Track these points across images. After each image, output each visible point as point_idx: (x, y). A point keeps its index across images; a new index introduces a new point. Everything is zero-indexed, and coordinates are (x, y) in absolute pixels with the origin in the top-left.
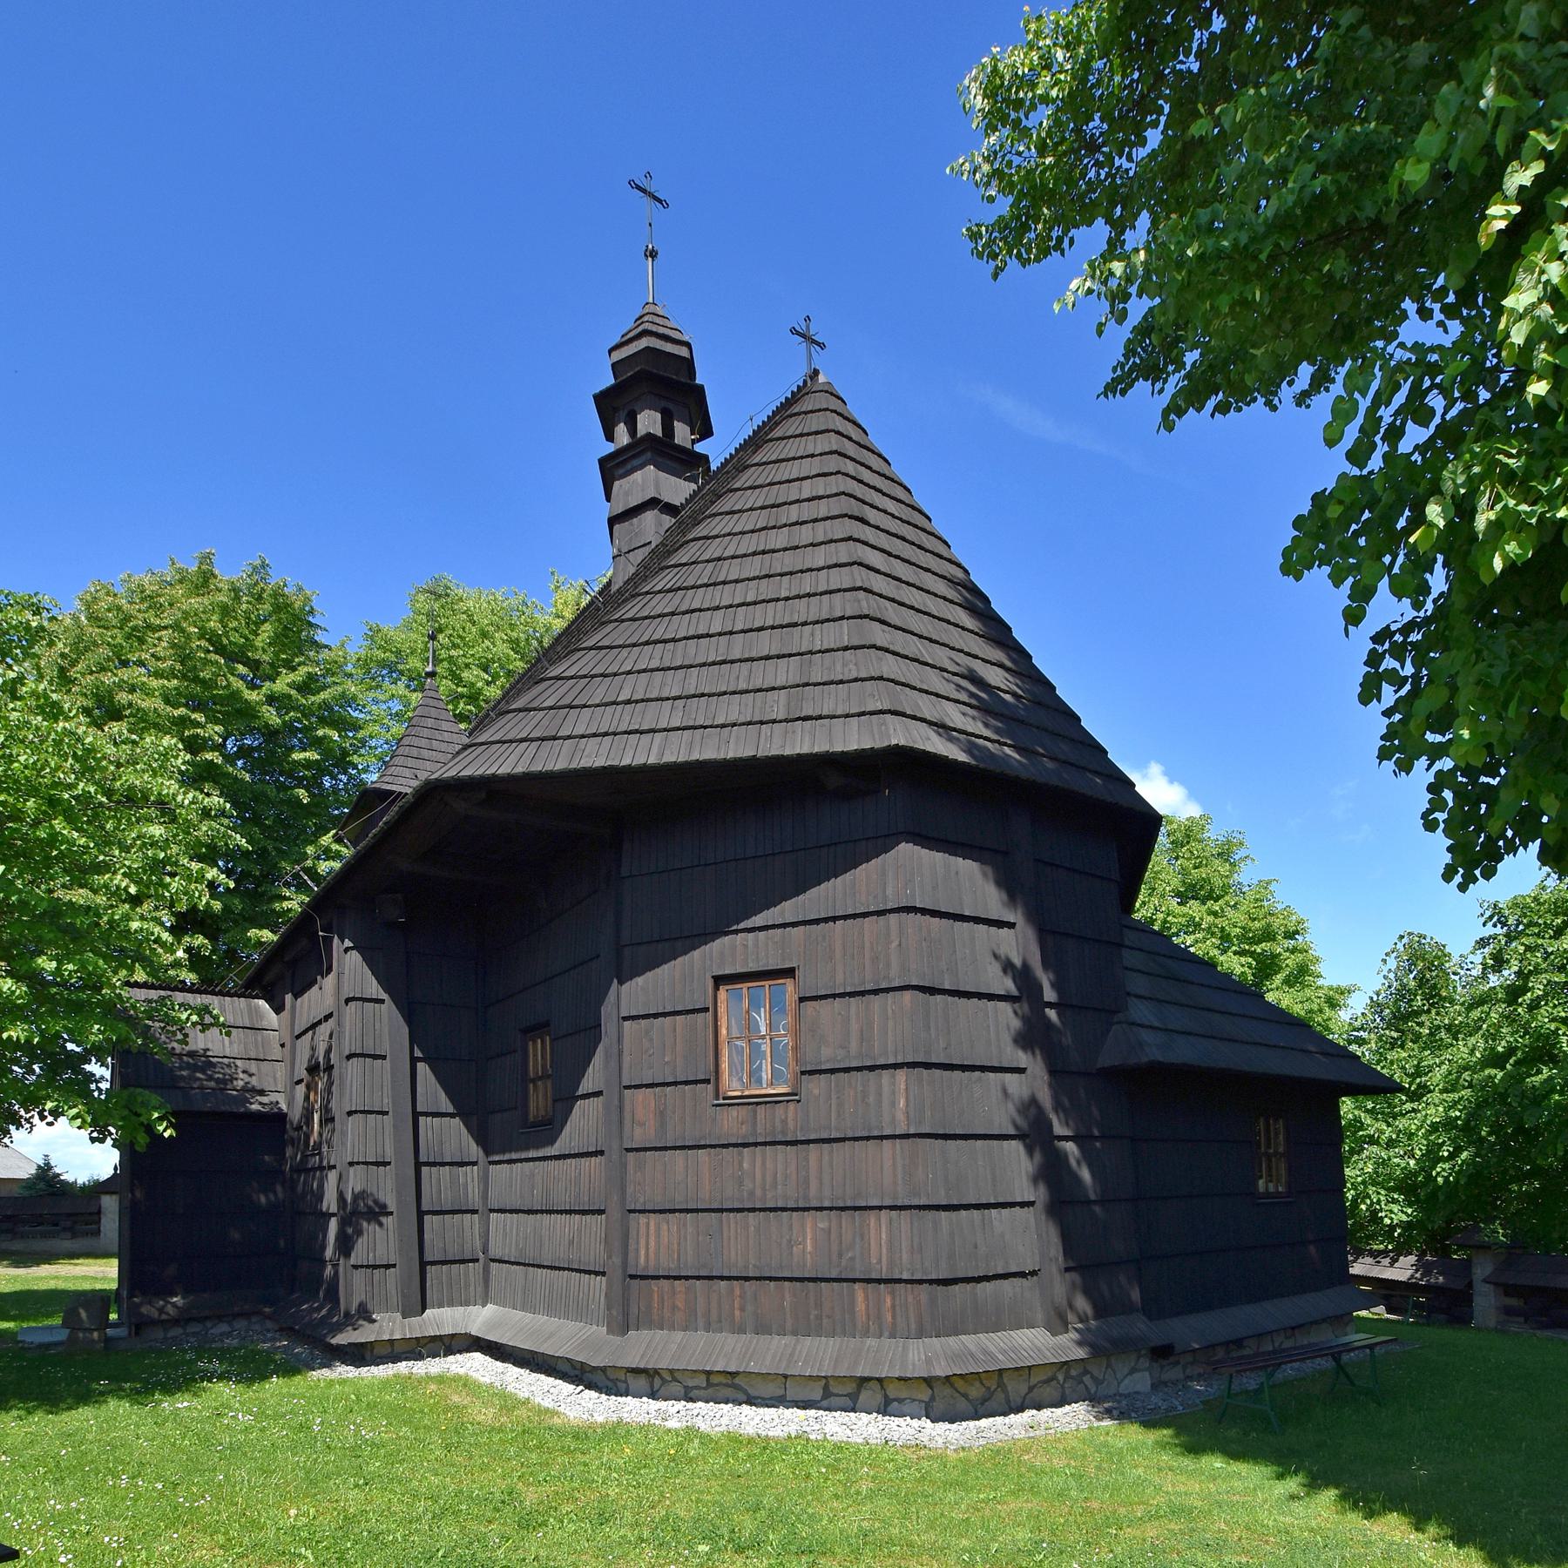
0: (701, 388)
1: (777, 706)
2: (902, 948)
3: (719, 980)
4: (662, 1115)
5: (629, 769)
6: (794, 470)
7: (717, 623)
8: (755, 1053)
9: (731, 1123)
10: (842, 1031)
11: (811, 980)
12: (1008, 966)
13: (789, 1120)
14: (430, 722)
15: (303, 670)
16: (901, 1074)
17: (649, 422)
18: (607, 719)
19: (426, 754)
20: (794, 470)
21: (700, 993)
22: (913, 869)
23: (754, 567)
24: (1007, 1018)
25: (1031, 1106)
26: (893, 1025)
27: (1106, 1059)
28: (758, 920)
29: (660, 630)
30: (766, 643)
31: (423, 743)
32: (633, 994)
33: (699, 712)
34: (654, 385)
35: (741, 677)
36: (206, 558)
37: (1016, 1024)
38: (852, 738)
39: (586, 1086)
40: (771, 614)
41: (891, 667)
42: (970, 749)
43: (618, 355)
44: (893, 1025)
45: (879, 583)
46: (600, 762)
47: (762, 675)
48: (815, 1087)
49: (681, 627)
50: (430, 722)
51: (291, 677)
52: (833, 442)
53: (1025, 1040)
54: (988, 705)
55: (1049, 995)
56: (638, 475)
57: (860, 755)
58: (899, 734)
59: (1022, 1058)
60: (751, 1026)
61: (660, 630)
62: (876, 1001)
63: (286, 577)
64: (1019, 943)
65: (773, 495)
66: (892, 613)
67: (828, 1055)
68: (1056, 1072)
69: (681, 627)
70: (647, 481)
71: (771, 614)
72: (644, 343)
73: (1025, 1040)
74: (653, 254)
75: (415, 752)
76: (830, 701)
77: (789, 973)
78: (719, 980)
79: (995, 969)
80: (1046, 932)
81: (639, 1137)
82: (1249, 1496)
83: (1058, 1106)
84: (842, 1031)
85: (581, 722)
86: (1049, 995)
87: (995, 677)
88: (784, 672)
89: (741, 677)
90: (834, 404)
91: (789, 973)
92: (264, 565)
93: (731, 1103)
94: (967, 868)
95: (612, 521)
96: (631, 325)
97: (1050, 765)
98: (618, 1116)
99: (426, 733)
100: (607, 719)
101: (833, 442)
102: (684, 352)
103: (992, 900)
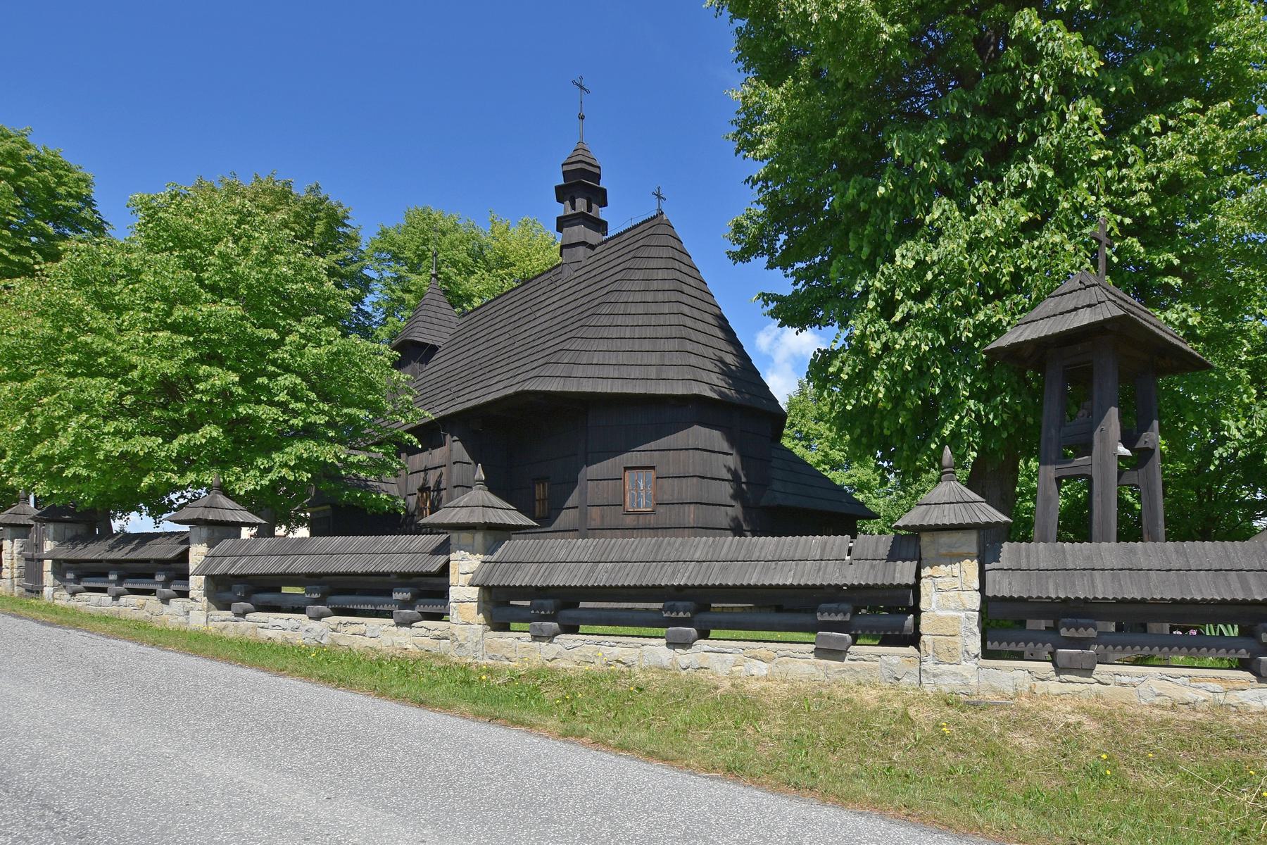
0: (605, 191)
1: (652, 373)
2: (694, 462)
3: (626, 469)
4: (602, 517)
5: (792, 587)
6: (653, 263)
7: (627, 333)
8: (639, 496)
9: (630, 521)
10: (671, 490)
11: (661, 471)
12: (729, 470)
13: (652, 520)
14: (435, 303)
15: (343, 254)
16: (692, 507)
17: (581, 205)
18: (591, 371)
19: (435, 321)
20: (653, 263)
21: (619, 472)
22: (699, 435)
23: (641, 309)
24: (728, 489)
25: (735, 519)
26: (689, 489)
27: (764, 502)
28: (641, 448)
29: (605, 333)
30: (647, 345)
31: (432, 314)
32: (593, 470)
33: (624, 372)
34: (581, 186)
35: (638, 358)
36: (288, 184)
37: (731, 491)
38: (680, 389)
39: (569, 503)
40: (648, 332)
41: (693, 360)
42: (720, 393)
43: (566, 168)
44: (689, 489)
45: (689, 322)
46: (589, 390)
47: (647, 359)
48: (662, 509)
49: (614, 332)
50: (435, 303)
51: (335, 257)
52: (670, 253)
53: (734, 497)
54: (726, 372)
55: (744, 479)
56: (575, 228)
57: (683, 395)
58: (696, 389)
59: (733, 503)
60: (638, 486)
61: (605, 333)
62: (684, 480)
63: (334, 196)
64: (733, 461)
65: (648, 274)
66: (693, 335)
67: (666, 498)
68: (745, 507)
69: (614, 332)
70: (579, 232)
71: (648, 332)
72: (579, 166)
73: (734, 497)
74: (582, 118)
75: (429, 320)
76: (672, 372)
77: (653, 468)
78: (626, 469)
79: (724, 471)
80: (744, 457)
81: (593, 524)
82: (900, 832)
83: (745, 520)
84: (671, 490)
85: (578, 371)
86: (744, 479)
87: (730, 359)
88: (654, 359)
89: (638, 358)
90: (668, 231)
91: (653, 468)
92: (317, 187)
93: (629, 513)
94: (717, 434)
95: (562, 247)
96: (570, 153)
97: (747, 396)
98: (584, 517)
99: (433, 309)
100: (591, 371)
101: (670, 253)
102: (597, 171)
103: (725, 446)
